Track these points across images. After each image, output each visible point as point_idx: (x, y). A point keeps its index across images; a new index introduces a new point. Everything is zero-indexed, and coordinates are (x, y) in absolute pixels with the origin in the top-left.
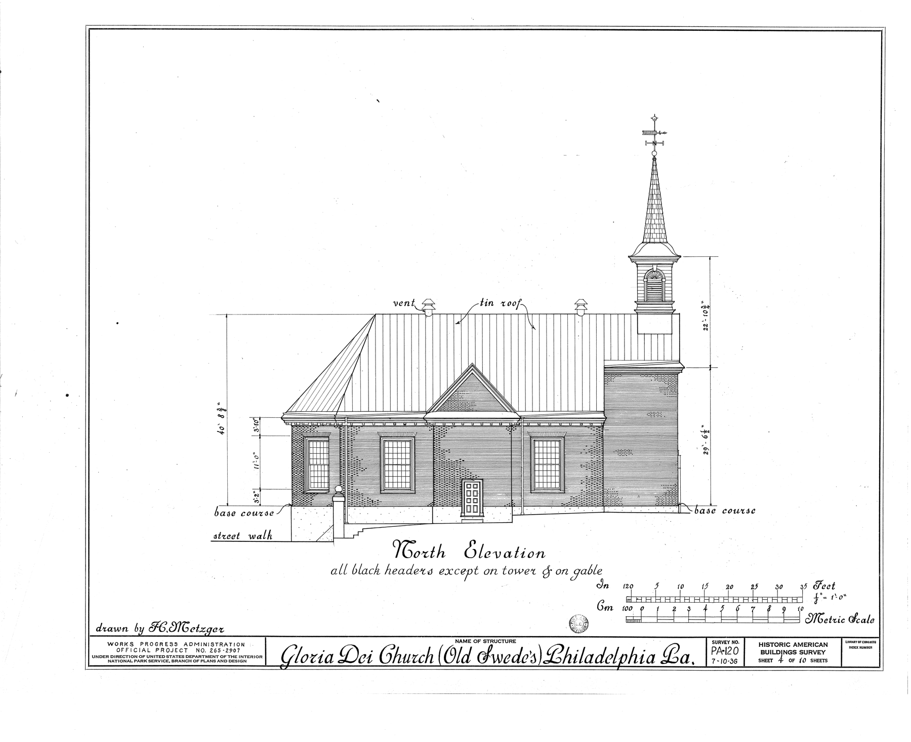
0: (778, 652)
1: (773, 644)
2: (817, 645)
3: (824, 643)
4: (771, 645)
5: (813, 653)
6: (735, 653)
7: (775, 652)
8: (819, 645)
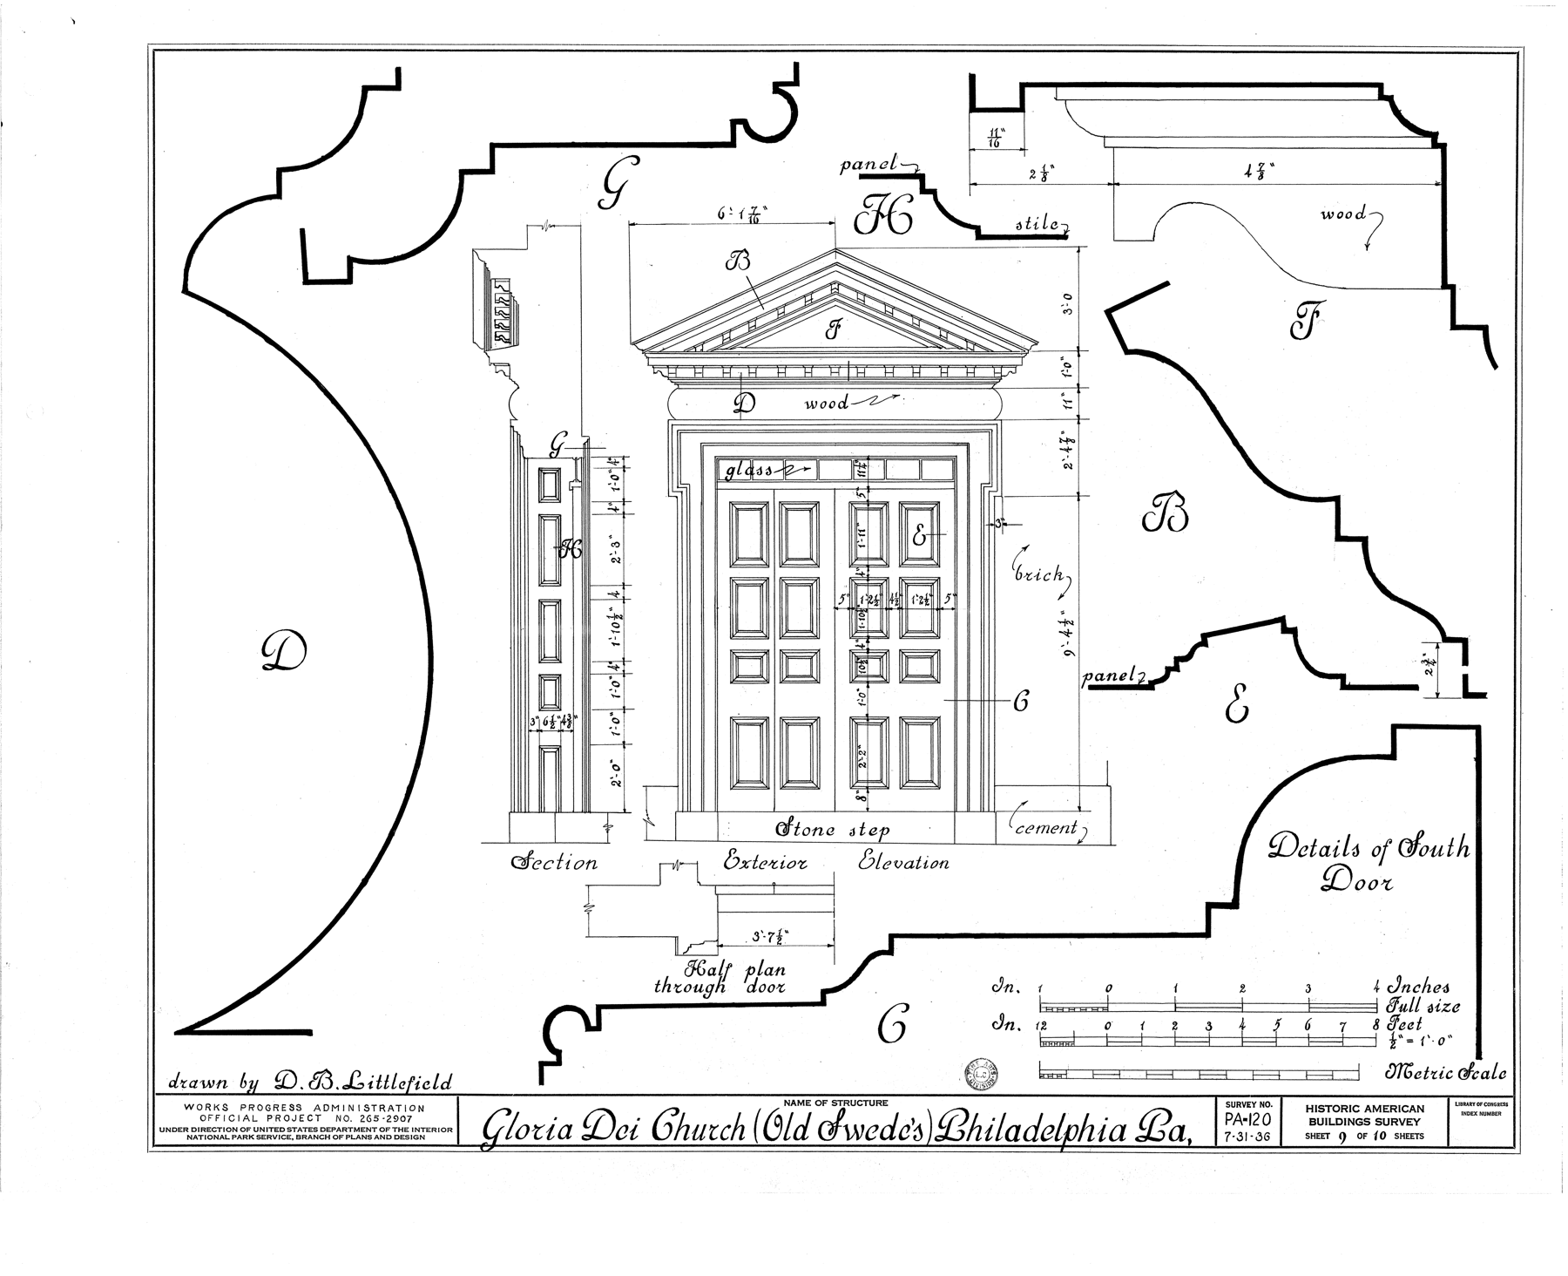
0: (1339, 1122)
1: (1331, 1108)
2: (1405, 1109)
3: (1418, 1106)
4: (1326, 1108)
5: (1399, 1123)
7: (1333, 1121)
8: (1409, 1109)
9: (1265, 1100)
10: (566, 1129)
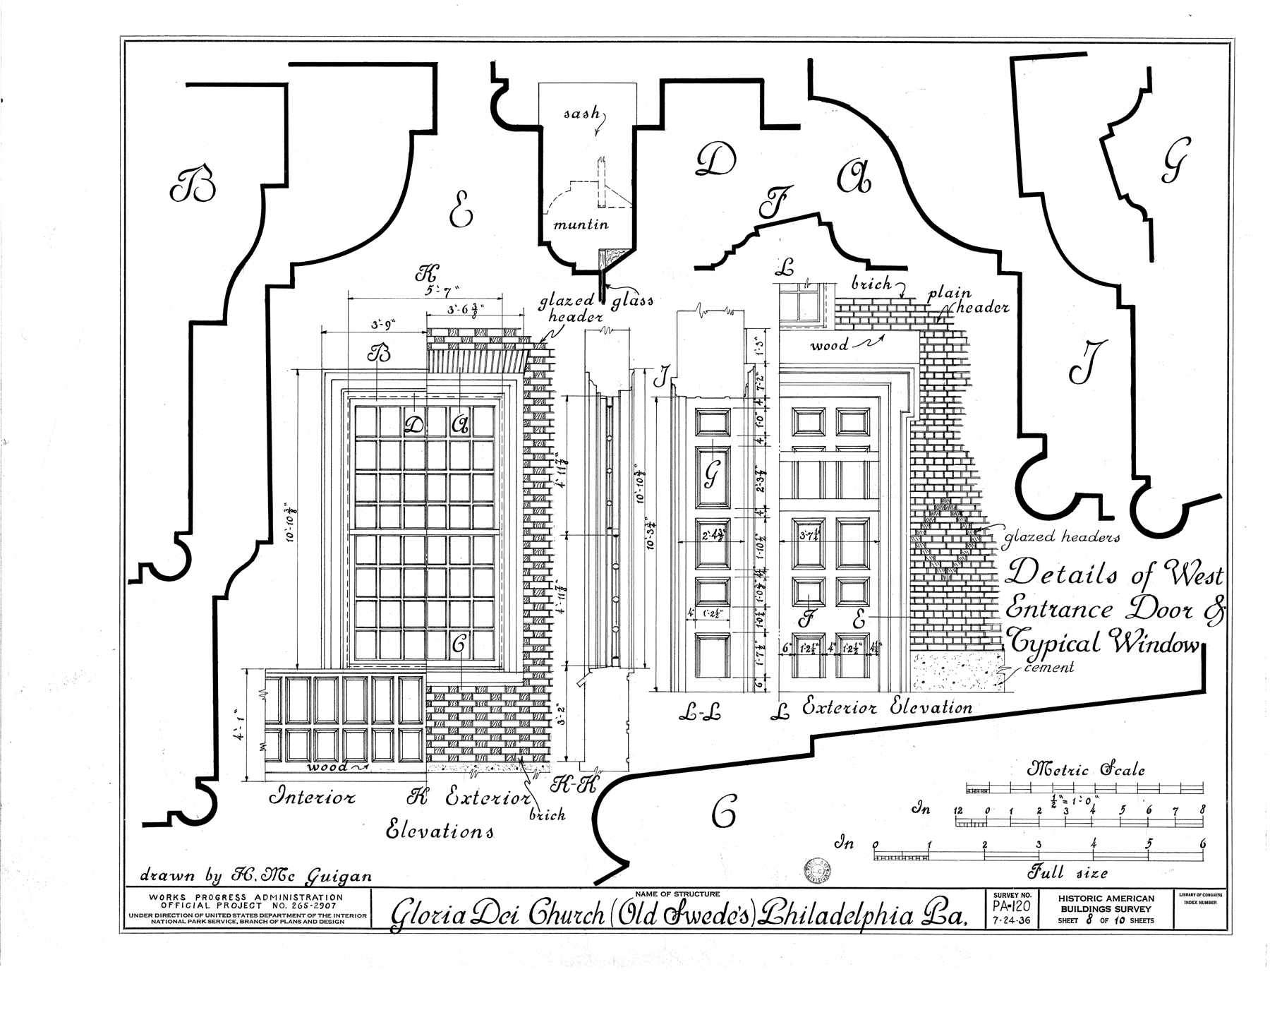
0: (1086, 909)
1: (1079, 898)
2: (1139, 899)
4: (1075, 898)
5: (1134, 910)
6: (1026, 909)
7: (1081, 909)
8: (1142, 899)
9: (1026, 891)
10: (460, 915)
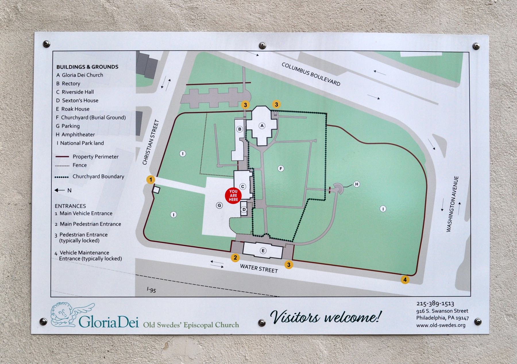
0: (71, 67)
4: (148, 150)
